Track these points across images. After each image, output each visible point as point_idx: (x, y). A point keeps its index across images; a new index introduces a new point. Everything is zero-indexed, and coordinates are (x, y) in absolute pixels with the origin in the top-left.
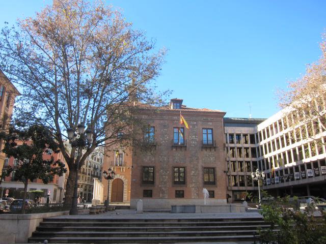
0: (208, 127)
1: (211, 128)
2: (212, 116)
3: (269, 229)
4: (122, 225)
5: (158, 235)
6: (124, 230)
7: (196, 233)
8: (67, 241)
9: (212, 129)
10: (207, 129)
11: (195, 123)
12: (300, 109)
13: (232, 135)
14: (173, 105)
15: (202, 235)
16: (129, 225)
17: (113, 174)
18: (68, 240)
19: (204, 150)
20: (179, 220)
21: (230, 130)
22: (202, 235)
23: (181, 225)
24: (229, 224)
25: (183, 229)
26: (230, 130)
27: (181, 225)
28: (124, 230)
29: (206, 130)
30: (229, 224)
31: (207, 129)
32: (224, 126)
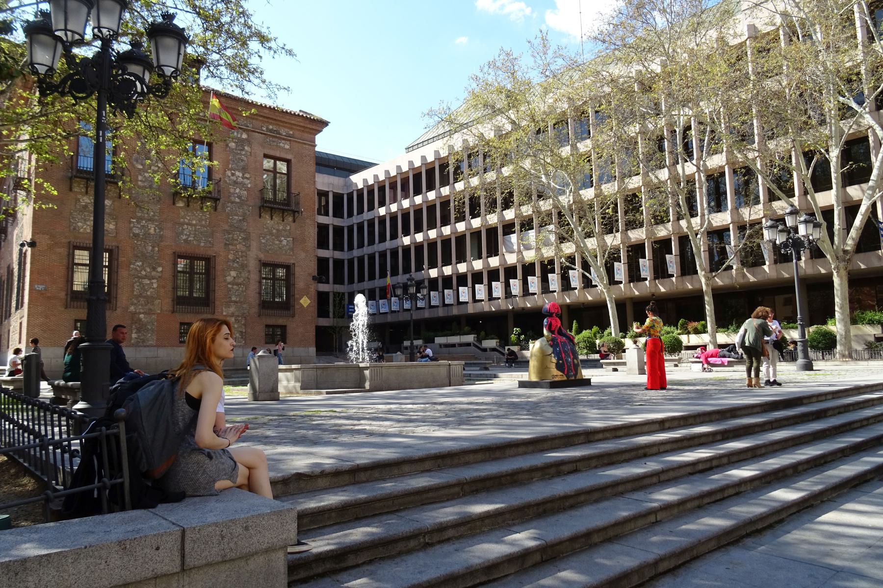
0: (278, 154)
1: (288, 157)
10: (276, 159)
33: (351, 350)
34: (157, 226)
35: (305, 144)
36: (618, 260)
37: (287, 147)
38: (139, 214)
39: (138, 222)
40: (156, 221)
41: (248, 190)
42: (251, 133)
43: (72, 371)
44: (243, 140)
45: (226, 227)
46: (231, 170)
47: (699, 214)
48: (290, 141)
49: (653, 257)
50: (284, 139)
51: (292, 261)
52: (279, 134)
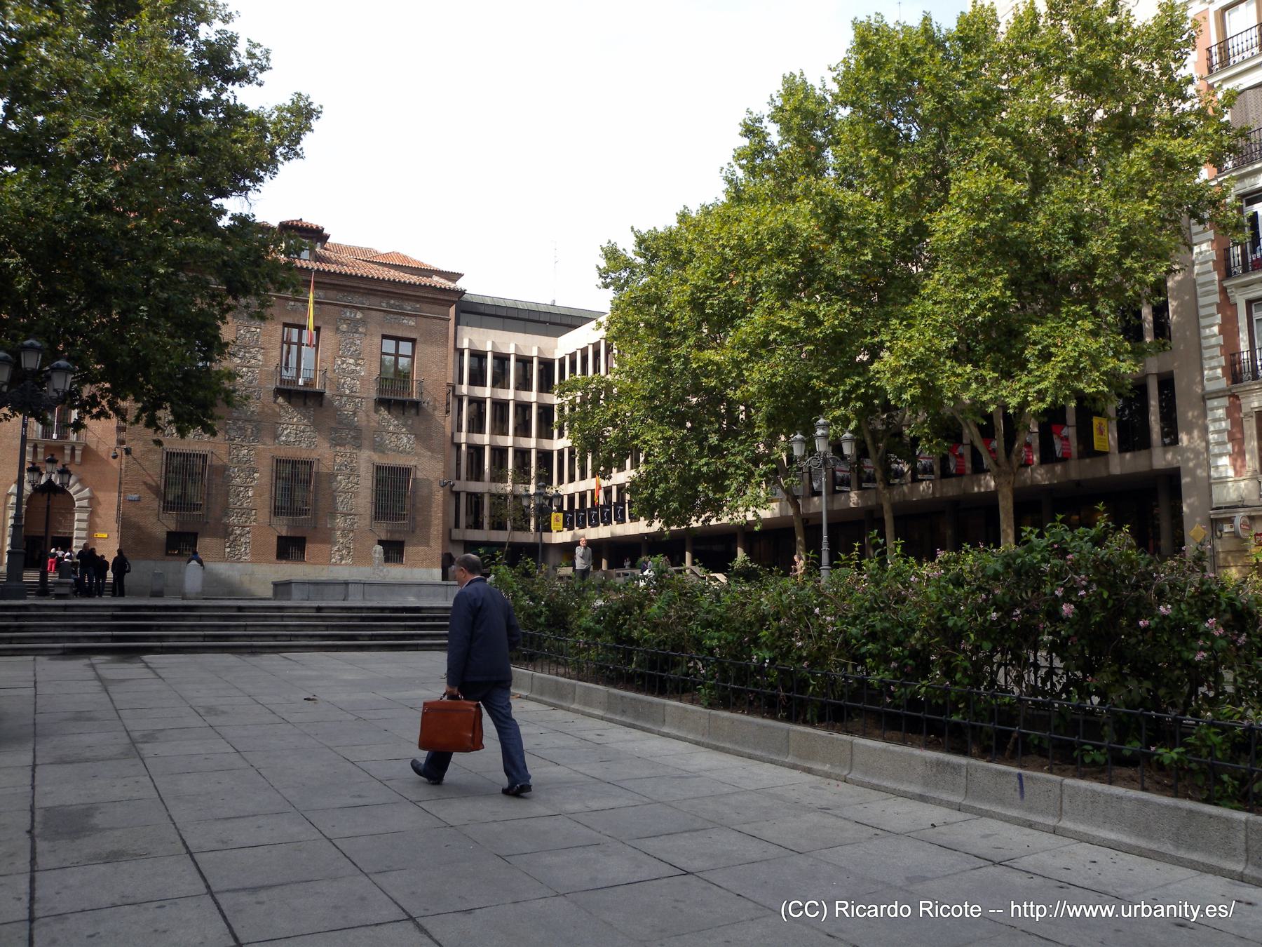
0: (400, 334)
1: (413, 336)
2: (417, 299)
3: (1047, 664)
4: (183, 618)
5: (275, 637)
6: (192, 628)
7: (360, 635)
8: (60, 652)
9: (413, 341)
10: (398, 339)
11: (359, 315)
12: (1088, 408)
13: (479, 356)
14: (6, 165)
15: (372, 637)
16: (201, 618)
17: (66, 477)
18: (63, 648)
19: (383, 412)
20: (319, 609)
21: (488, 340)
22: (372, 637)
23: (323, 618)
24: (433, 619)
25: (327, 627)
26: (488, 340)
27: (323, 618)
28: (192, 628)
29: (393, 342)
30: (433, 619)
31: (398, 339)
32: (457, 323)
33: (435, 409)
34: (255, 427)
35: (435, 318)
36: (1063, 423)
37: (412, 323)
38: (235, 415)
39: (235, 424)
40: (255, 421)
41: (362, 379)
42: (366, 312)
43: (681, 428)
44: (358, 320)
45: (334, 425)
46: (341, 357)
47: (62, 580)
48: (415, 316)
49: (1077, 422)
50: (408, 315)
51: (413, 463)
52: (402, 309)
